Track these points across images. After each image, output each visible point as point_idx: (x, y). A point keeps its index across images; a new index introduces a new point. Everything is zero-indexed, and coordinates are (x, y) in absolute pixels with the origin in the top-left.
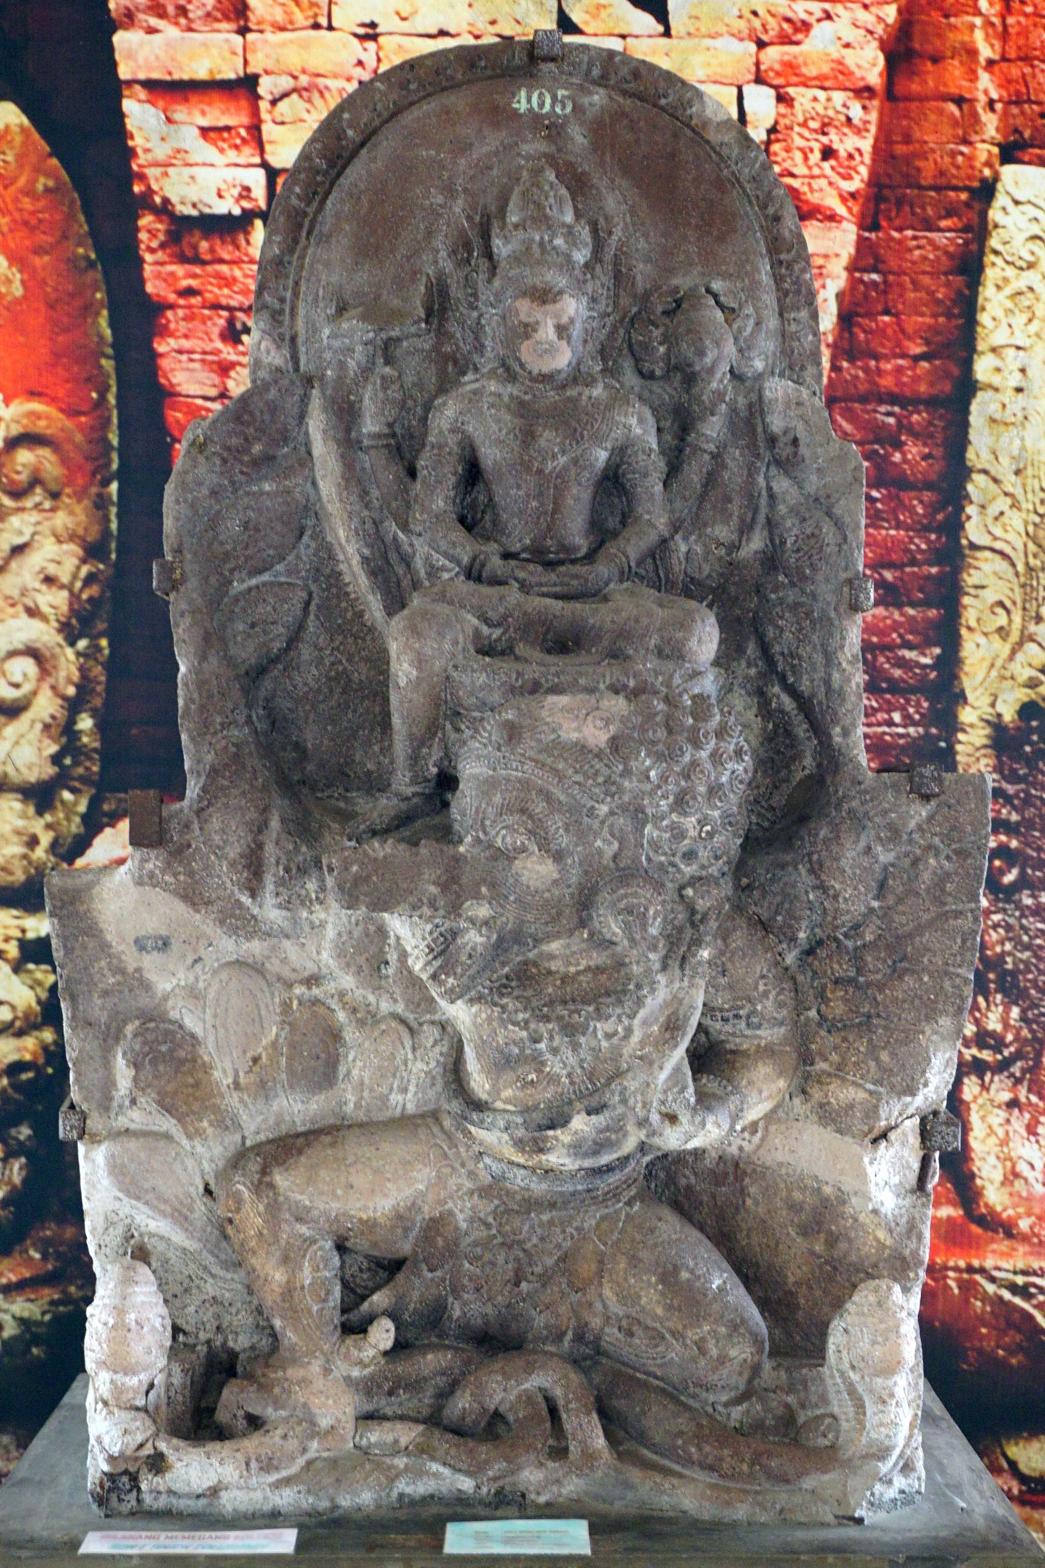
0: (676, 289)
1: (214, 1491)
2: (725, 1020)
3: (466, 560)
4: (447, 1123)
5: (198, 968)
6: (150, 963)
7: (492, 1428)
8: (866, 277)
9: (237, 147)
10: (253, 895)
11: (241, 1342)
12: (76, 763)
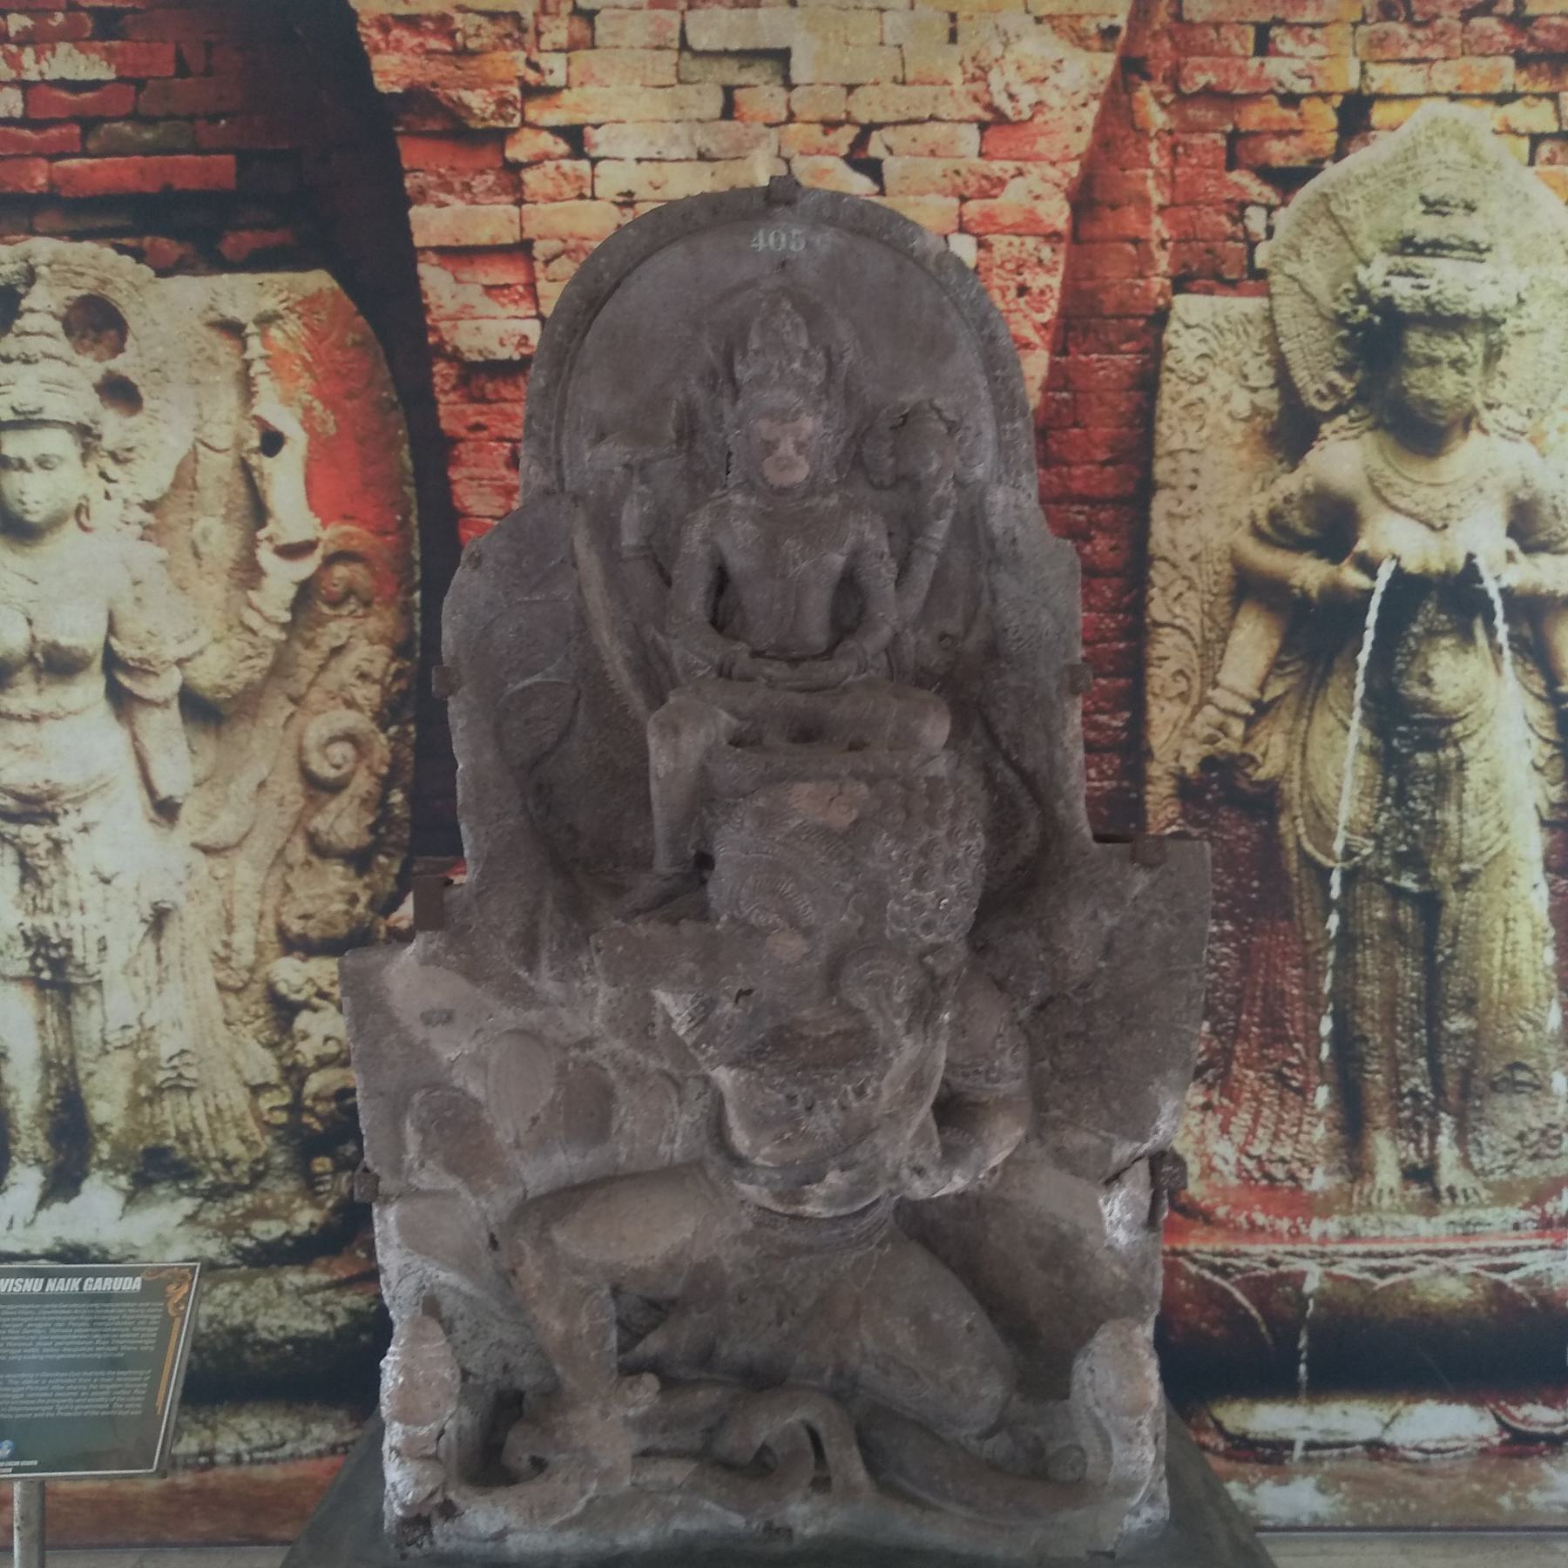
0: (903, 406)
1: (500, 1536)
2: (966, 1076)
3: (717, 658)
4: (712, 1172)
5: (481, 1037)
6: (436, 1035)
7: (761, 1467)
8: (1058, 396)
9: (515, 302)
10: (530, 969)
11: (527, 1380)
12: (389, 832)
